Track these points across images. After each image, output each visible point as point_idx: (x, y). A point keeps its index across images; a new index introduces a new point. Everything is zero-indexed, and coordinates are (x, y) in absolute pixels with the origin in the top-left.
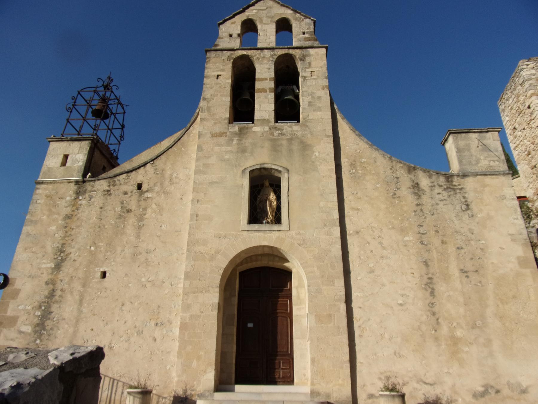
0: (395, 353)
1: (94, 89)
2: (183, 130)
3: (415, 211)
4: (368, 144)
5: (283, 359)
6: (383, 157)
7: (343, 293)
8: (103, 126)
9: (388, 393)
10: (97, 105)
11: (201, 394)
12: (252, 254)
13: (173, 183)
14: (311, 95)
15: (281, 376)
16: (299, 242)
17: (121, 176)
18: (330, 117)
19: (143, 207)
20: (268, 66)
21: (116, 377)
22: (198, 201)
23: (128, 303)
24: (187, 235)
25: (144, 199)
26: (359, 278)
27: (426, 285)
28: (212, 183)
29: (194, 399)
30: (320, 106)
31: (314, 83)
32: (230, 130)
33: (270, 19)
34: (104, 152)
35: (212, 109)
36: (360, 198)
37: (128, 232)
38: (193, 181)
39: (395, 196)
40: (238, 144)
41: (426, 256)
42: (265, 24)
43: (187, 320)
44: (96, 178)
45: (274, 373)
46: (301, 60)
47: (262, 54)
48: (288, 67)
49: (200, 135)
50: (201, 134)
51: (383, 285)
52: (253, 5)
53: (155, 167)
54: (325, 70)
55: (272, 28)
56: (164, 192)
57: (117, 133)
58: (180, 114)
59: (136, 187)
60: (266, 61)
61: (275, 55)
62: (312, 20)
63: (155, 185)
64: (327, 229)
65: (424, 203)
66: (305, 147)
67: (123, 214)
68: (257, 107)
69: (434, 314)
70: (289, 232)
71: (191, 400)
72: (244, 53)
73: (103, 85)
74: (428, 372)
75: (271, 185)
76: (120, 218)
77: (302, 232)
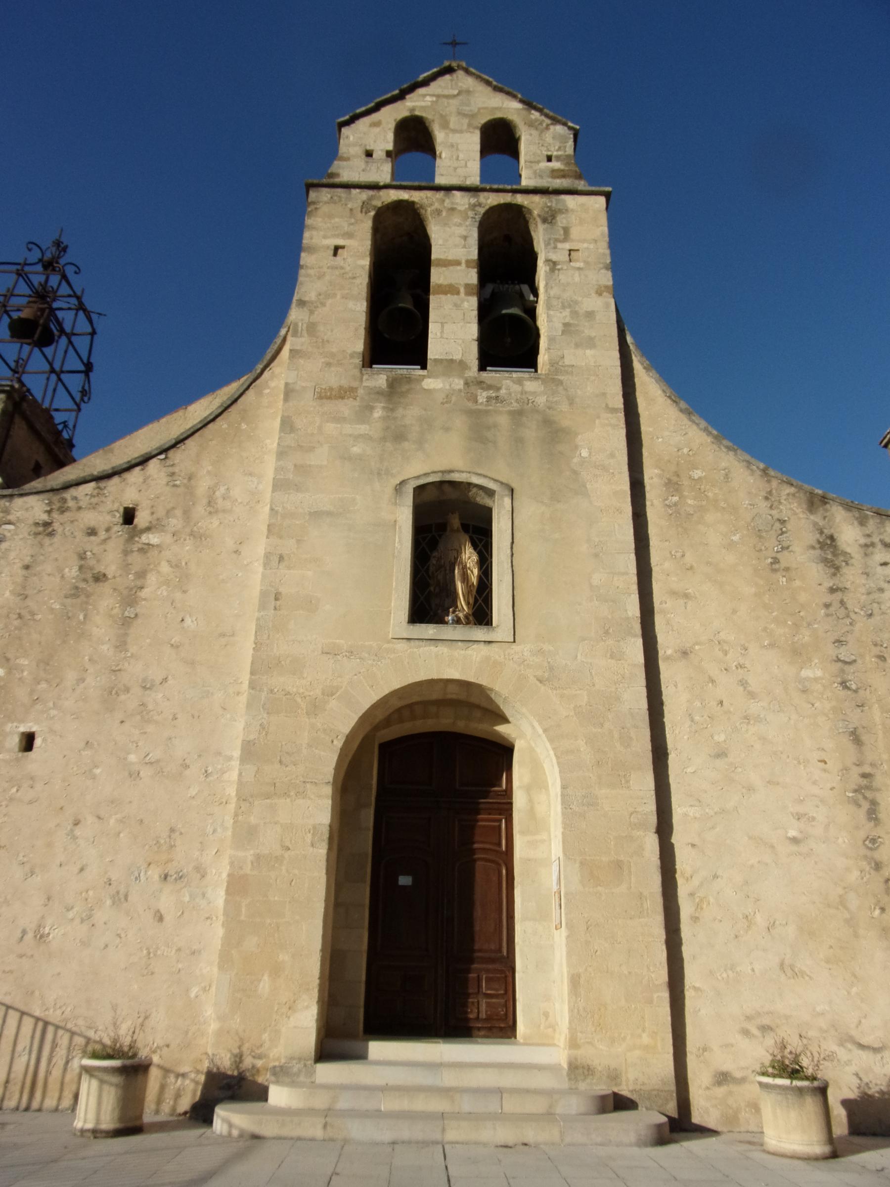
0: (782, 965)
1: (19, 267)
2: (245, 380)
3: (827, 606)
4: (709, 433)
5: (487, 971)
6: (748, 467)
7: (651, 807)
8: (37, 361)
9: (786, 1082)
10: (23, 308)
11: (281, 1067)
12: (416, 699)
13: (217, 512)
14: (570, 306)
15: (483, 1015)
16: (539, 673)
17: (82, 488)
18: (618, 363)
19: (136, 568)
20: (462, 231)
21: (54, 1016)
22: (281, 558)
23: (90, 819)
24: (249, 645)
25: (141, 550)
26: (689, 770)
27: (855, 791)
28: (316, 515)
29: (260, 1080)
30: (593, 334)
31: (577, 279)
32: (365, 384)
33: (466, 121)
34: (38, 426)
35: (321, 328)
36: (691, 568)
37: (95, 631)
38: (267, 509)
39: (777, 566)
40: (384, 419)
41: (855, 718)
42: (455, 131)
43: (247, 869)
44: (16, 491)
45: (465, 1005)
46: (545, 221)
47: (447, 201)
48: (508, 238)
49: (289, 392)
50: (293, 391)
51: (750, 789)
52: (425, 83)
53: (171, 469)
54: (603, 249)
55: (473, 142)
56: (192, 534)
57: (75, 382)
58: (235, 337)
59: (119, 517)
60: (457, 219)
61: (480, 205)
62: (570, 128)
63: (169, 513)
64: (610, 642)
65: (848, 585)
66: (555, 435)
67: (82, 585)
68: (433, 329)
69: (878, 866)
70: (514, 646)
71: (255, 1083)
72: (404, 195)
73: (40, 260)
74: (865, 1017)
75: (465, 528)
76: (75, 596)
77: (547, 647)
